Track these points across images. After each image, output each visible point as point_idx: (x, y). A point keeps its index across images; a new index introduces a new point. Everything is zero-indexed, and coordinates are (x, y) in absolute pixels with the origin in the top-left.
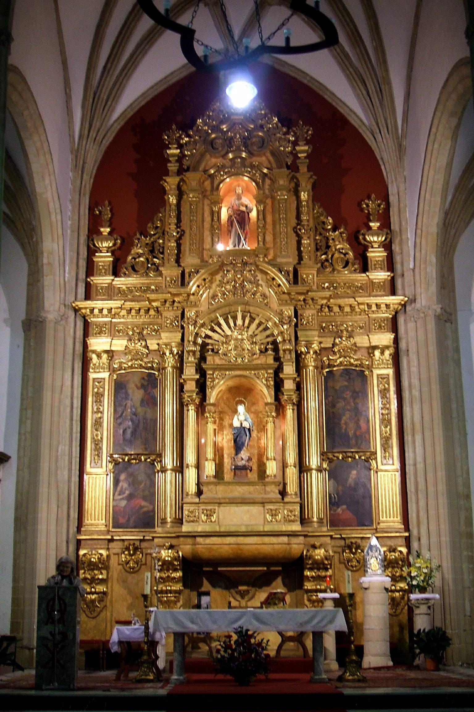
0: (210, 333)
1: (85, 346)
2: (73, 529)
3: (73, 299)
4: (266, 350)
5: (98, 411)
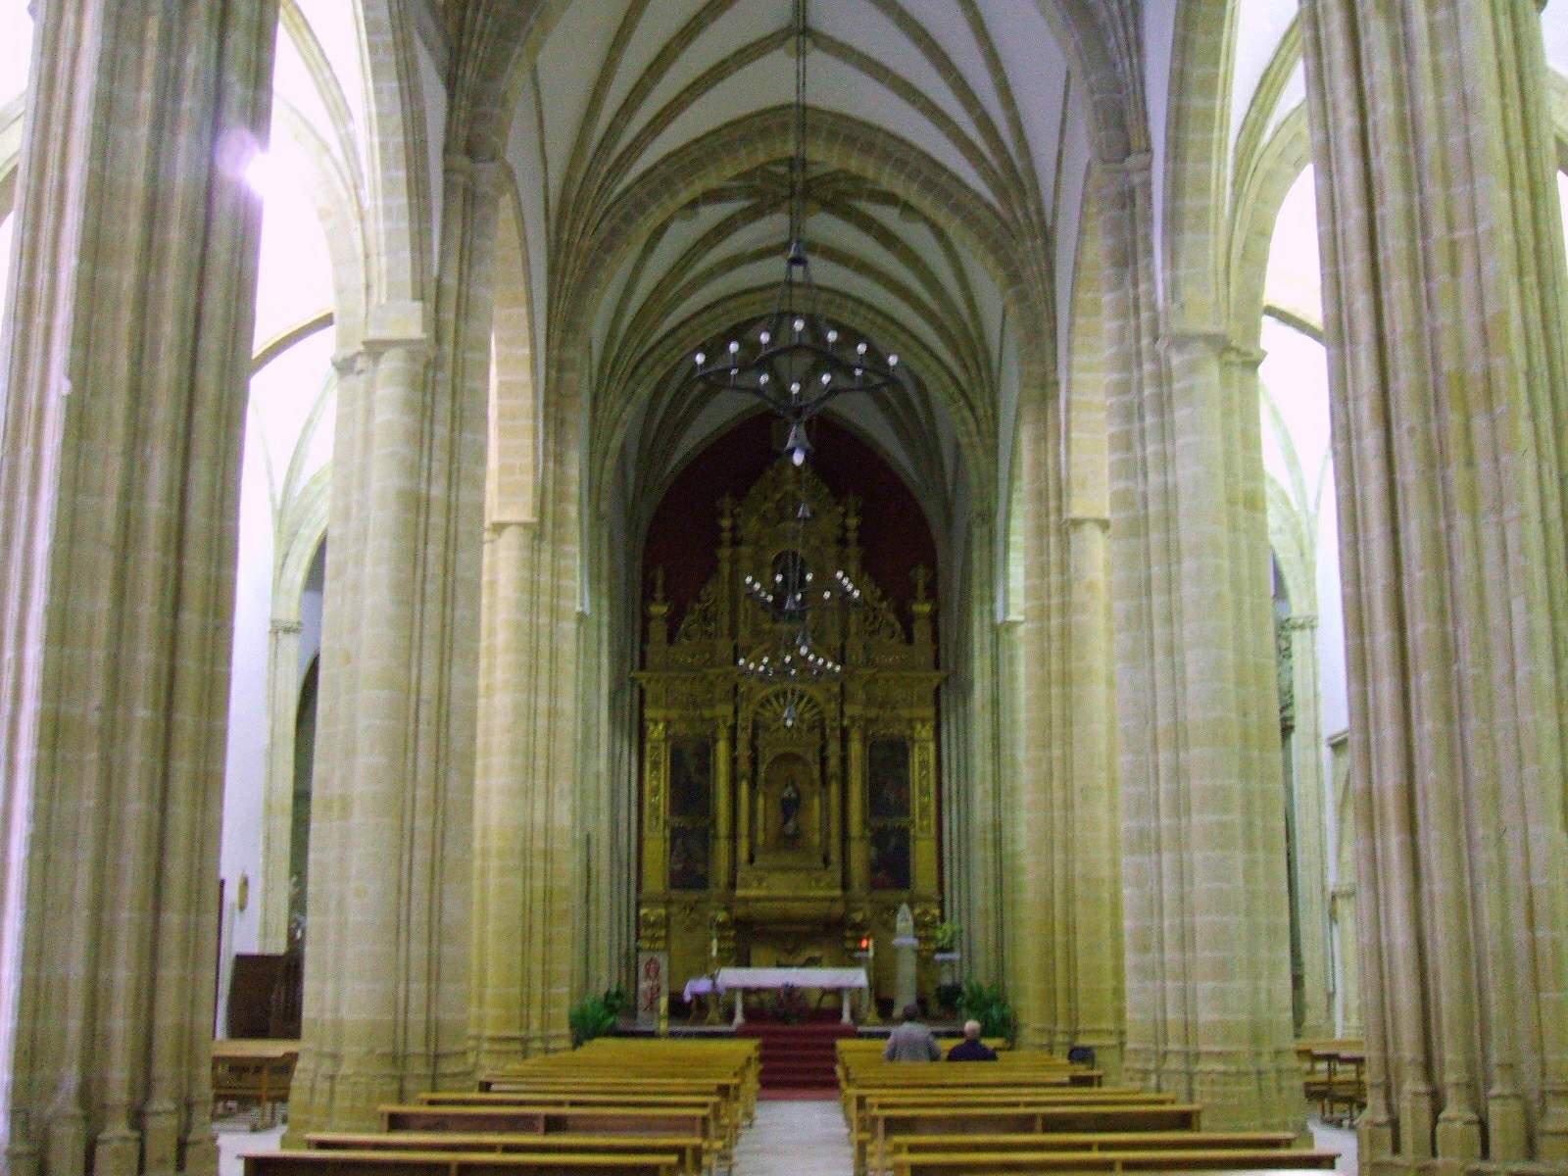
1: (641, 714)
4: (814, 728)
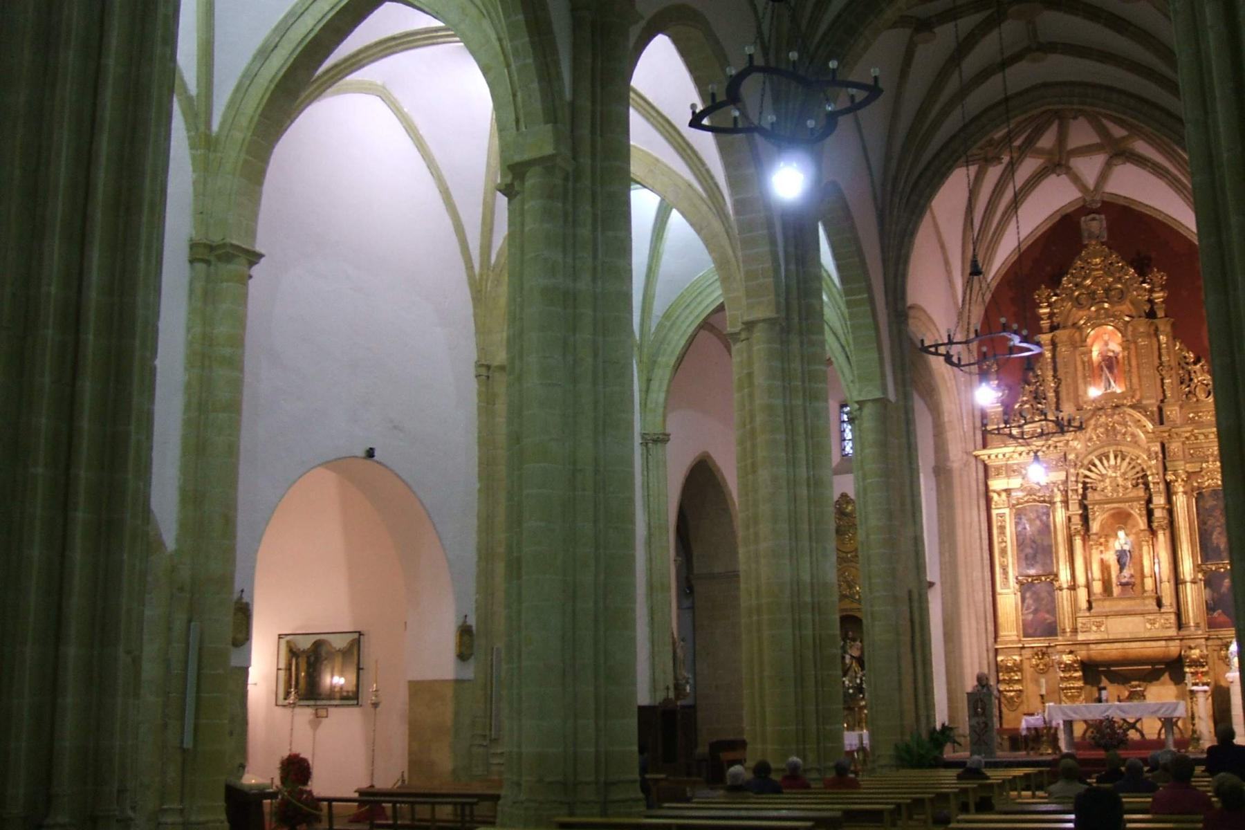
0: (1087, 473)
1: (987, 486)
2: (991, 640)
3: (973, 448)
4: (1137, 484)
5: (1003, 541)
